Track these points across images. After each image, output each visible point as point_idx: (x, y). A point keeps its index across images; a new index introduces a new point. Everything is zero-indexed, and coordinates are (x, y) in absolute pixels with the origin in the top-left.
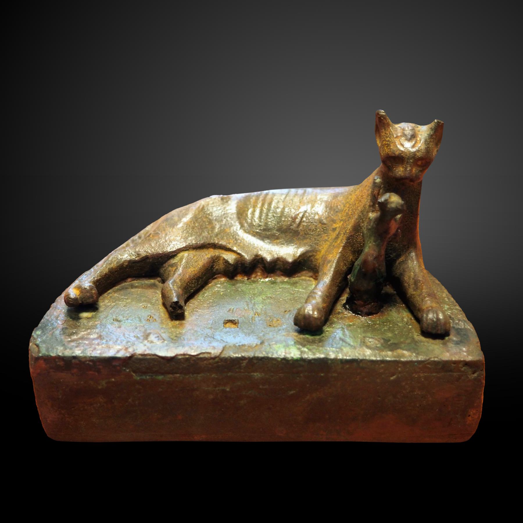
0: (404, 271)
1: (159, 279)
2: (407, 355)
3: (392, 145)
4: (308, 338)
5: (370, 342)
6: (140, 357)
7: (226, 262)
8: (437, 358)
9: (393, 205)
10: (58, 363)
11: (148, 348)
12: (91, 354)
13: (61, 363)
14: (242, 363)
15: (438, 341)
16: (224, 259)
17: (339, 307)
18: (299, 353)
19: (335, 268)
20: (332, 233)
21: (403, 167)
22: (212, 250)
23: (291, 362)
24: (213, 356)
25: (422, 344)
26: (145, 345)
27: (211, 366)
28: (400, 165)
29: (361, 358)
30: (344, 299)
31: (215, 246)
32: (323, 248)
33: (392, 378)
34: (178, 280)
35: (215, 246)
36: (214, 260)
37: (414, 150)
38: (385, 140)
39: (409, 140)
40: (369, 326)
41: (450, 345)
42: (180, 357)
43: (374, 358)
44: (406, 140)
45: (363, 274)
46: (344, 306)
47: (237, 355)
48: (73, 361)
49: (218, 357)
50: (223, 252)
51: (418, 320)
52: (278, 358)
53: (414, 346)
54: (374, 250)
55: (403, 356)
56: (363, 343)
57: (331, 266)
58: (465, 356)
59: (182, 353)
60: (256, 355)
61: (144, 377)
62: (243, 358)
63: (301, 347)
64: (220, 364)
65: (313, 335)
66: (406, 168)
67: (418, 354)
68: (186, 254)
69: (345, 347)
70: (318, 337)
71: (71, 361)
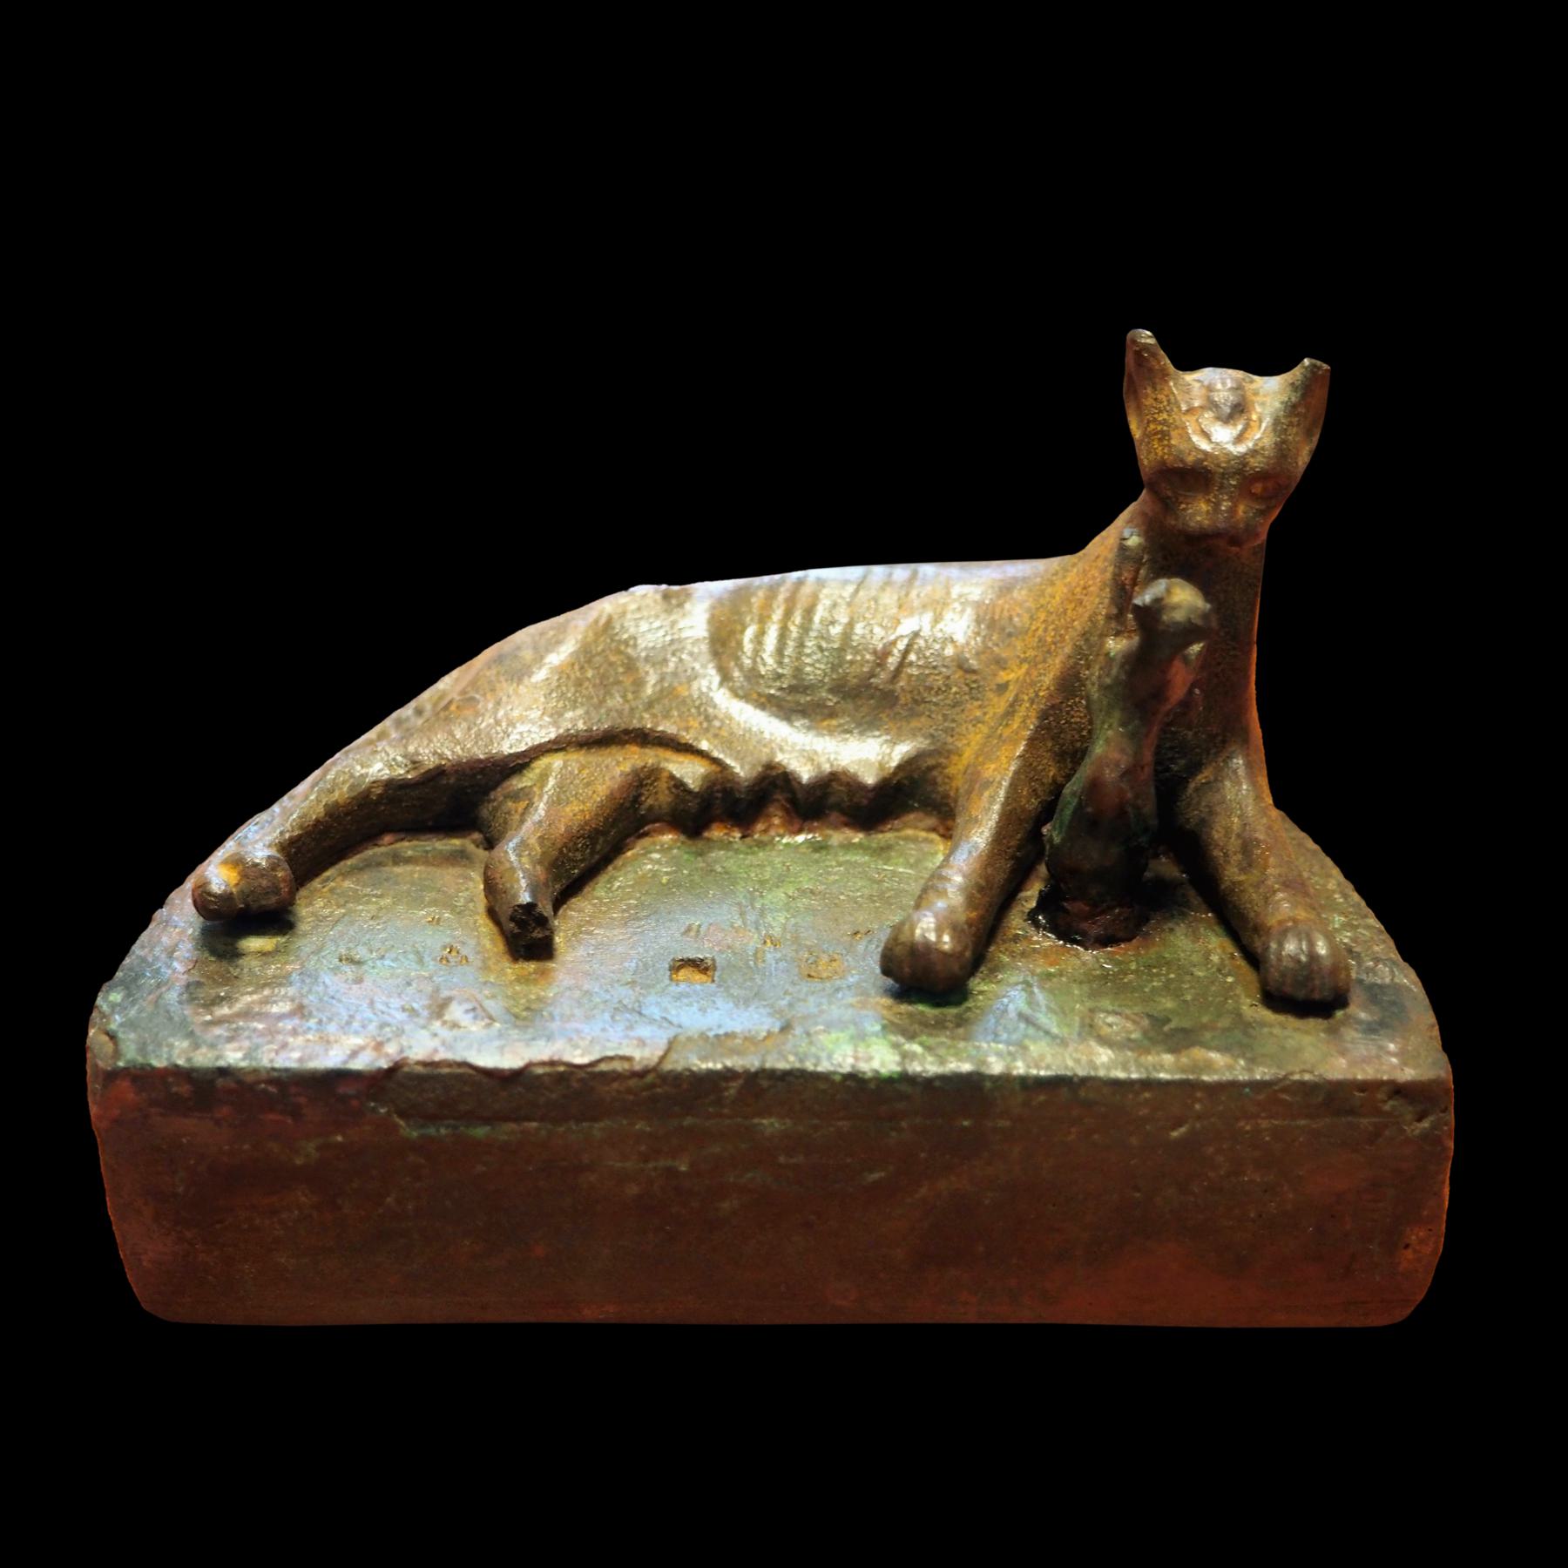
0: (1211, 813)
1: (477, 836)
2: (1220, 1065)
3: (1174, 434)
4: (922, 1013)
5: (1110, 1025)
6: (420, 1069)
7: (679, 785)
8: (1311, 1072)
9: (1179, 616)
10: (174, 1089)
11: (443, 1043)
12: (272, 1061)
13: (184, 1089)
14: (727, 1089)
15: (1312, 1023)
16: (672, 777)
17: (1016, 922)
18: (897, 1058)
19: (1005, 804)
20: (996, 700)
21: (1209, 501)
22: (634, 748)
23: (872, 1086)
24: (637, 1067)
25: (1266, 1030)
26: (435, 1035)
27: (631, 1097)
28: (1200, 496)
29: (1081, 1072)
30: (1031, 895)
31: (644, 738)
32: (970, 743)
33: (1175, 1134)
34: (533, 841)
35: (644, 738)
36: (642, 780)
37: (1241, 449)
38: (1155, 420)
39: (1227, 420)
40: (1105, 977)
41: (1350, 1034)
42: (540, 1071)
43: (1120, 1074)
44: (1218, 418)
45: (1089, 822)
46: (1032, 916)
47: (710, 1065)
48: (220, 1082)
49: (654, 1069)
50: (669, 754)
51: (1254, 959)
52: (835, 1073)
53: (1240, 1038)
54: (1123, 751)
55: (1209, 1066)
56: (1089, 1029)
57: (992, 799)
58: (1394, 1067)
59: (545, 1057)
60: (768, 1065)
61: (432, 1131)
62: (728, 1075)
63: (902, 1040)
64: (659, 1090)
65: (937, 1005)
66: (1217, 505)
67: (1252, 1062)
68: (556, 762)
69: (1034, 1040)
70: (952, 1011)
71: (212, 1082)
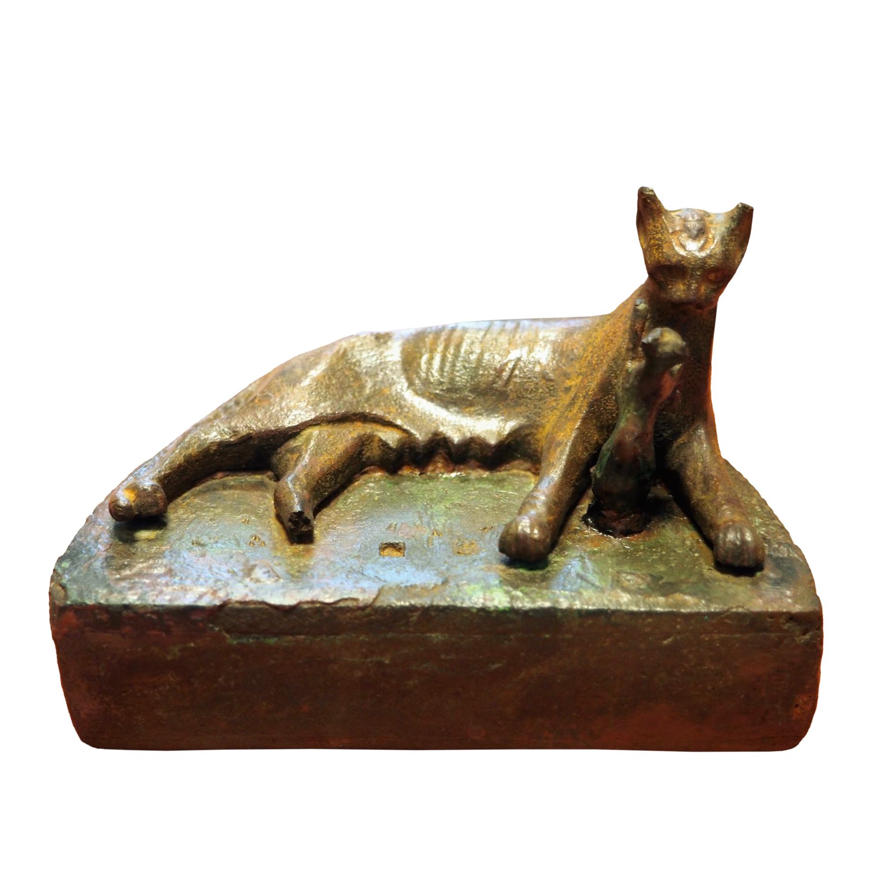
0: (686, 460)
1: (270, 473)
2: (691, 603)
3: (665, 246)
4: (522, 574)
5: (629, 581)
6: (238, 605)
7: (384, 444)
8: (743, 607)
9: (668, 349)
10: (99, 617)
11: (251, 591)
12: (154, 601)
13: (104, 617)
14: (412, 617)
15: (743, 579)
16: (381, 440)
17: (575, 522)
18: (508, 599)
19: (569, 455)
20: (564, 396)
21: (684, 284)
22: (359, 424)
23: (494, 615)
24: (361, 605)
25: (717, 583)
26: (247, 586)
27: (358, 622)
28: (680, 281)
29: (612, 607)
30: (584, 507)
31: (365, 418)
32: (549, 421)
33: (665, 642)
34: (302, 476)
35: (365, 418)
36: (363, 442)
37: (703, 254)
38: (654, 238)
39: (695, 238)
40: (626, 553)
41: (765, 586)
42: (306, 606)
43: (634, 608)
44: (690, 237)
45: (617, 466)
46: (584, 519)
47: (402, 603)
48: (125, 613)
49: (371, 606)
50: (379, 427)
51: (710, 543)
52: (473, 608)
53: (702, 588)
54: (636, 425)
55: (685, 604)
56: (617, 583)
57: (562, 452)
58: (789, 604)
59: (309, 599)
60: (435, 603)
61: (244, 640)
62: (413, 609)
63: (511, 589)
64: (373, 617)
65: (531, 569)
66: (689, 286)
67: (709, 601)
68: (315, 431)
69: (586, 589)
70: (539, 573)
71: (120, 613)
